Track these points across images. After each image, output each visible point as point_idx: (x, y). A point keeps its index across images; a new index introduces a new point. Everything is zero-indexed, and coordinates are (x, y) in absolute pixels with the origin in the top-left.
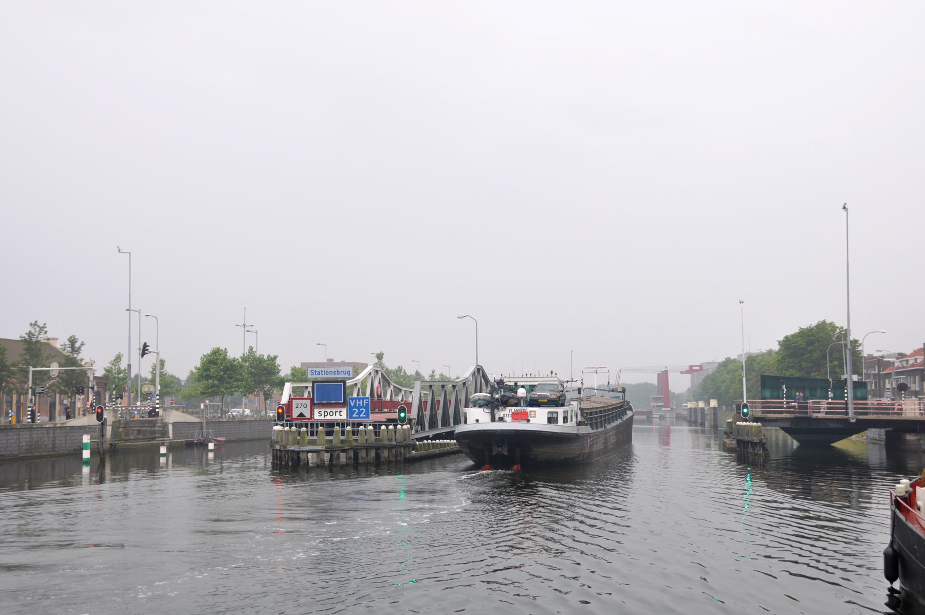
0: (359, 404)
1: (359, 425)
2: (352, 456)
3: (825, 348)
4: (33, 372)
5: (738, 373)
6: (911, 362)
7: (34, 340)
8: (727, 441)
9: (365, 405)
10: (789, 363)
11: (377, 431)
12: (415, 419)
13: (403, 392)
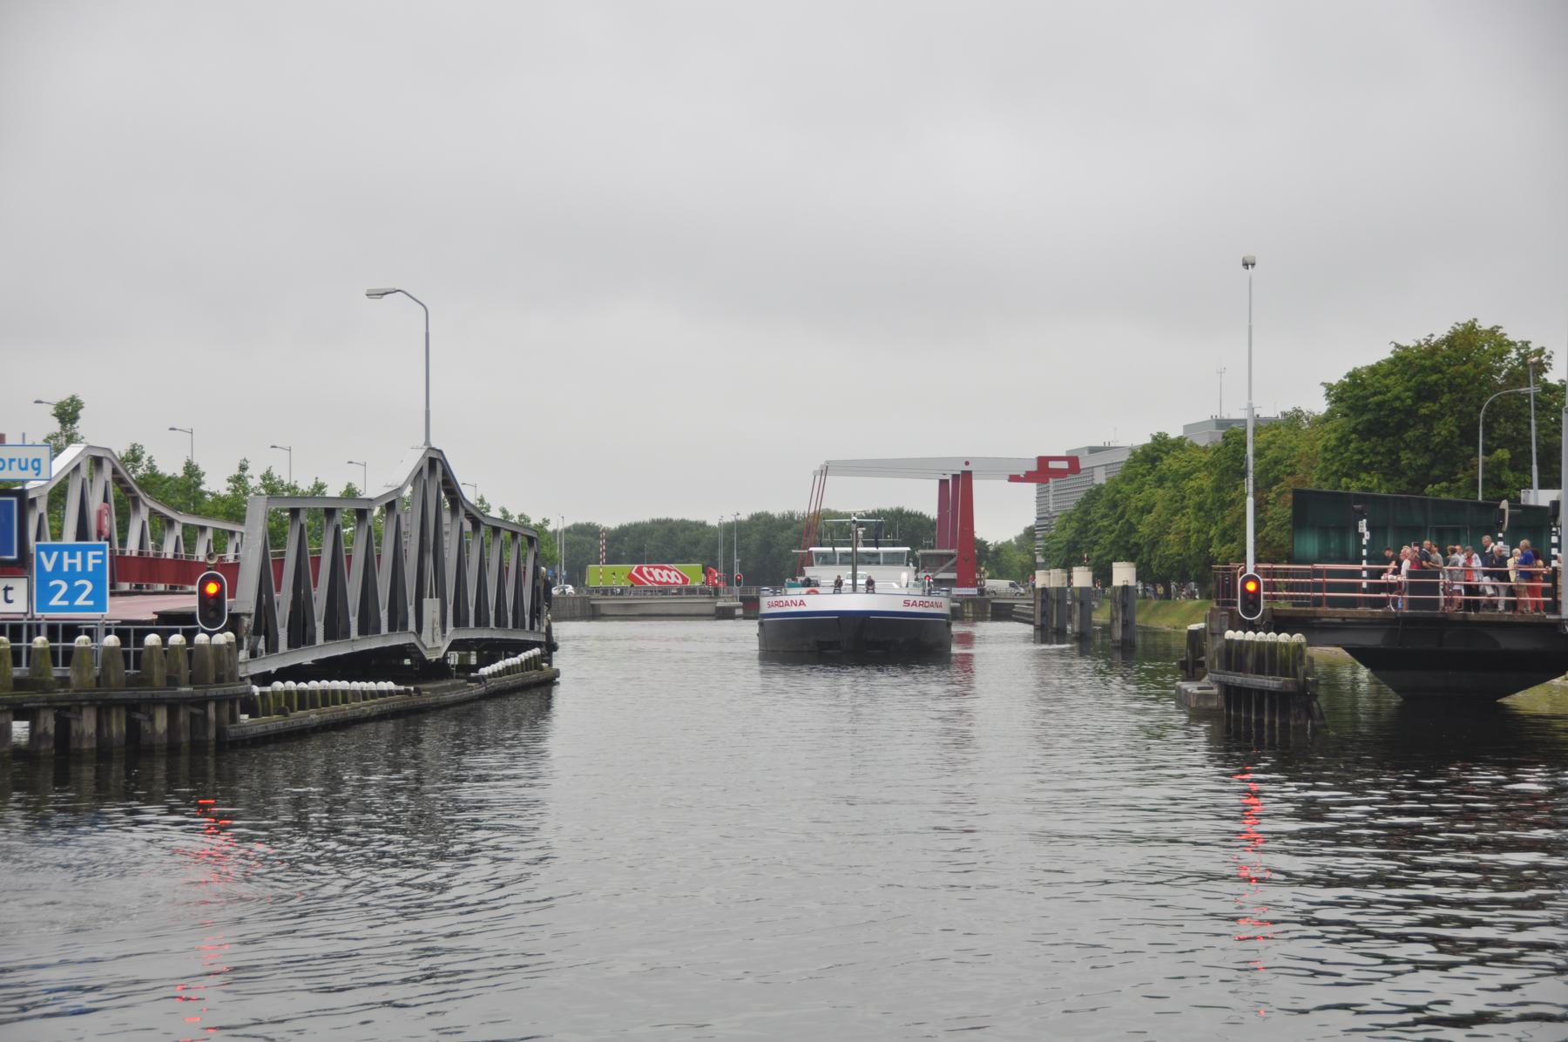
0: (72, 566)
1: (72, 631)
2: (52, 731)
3: (1472, 408)
5: (1192, 483)
9: (90, 569)
10: (1361, 452)
11: (129, 652)
12: (249, 615)
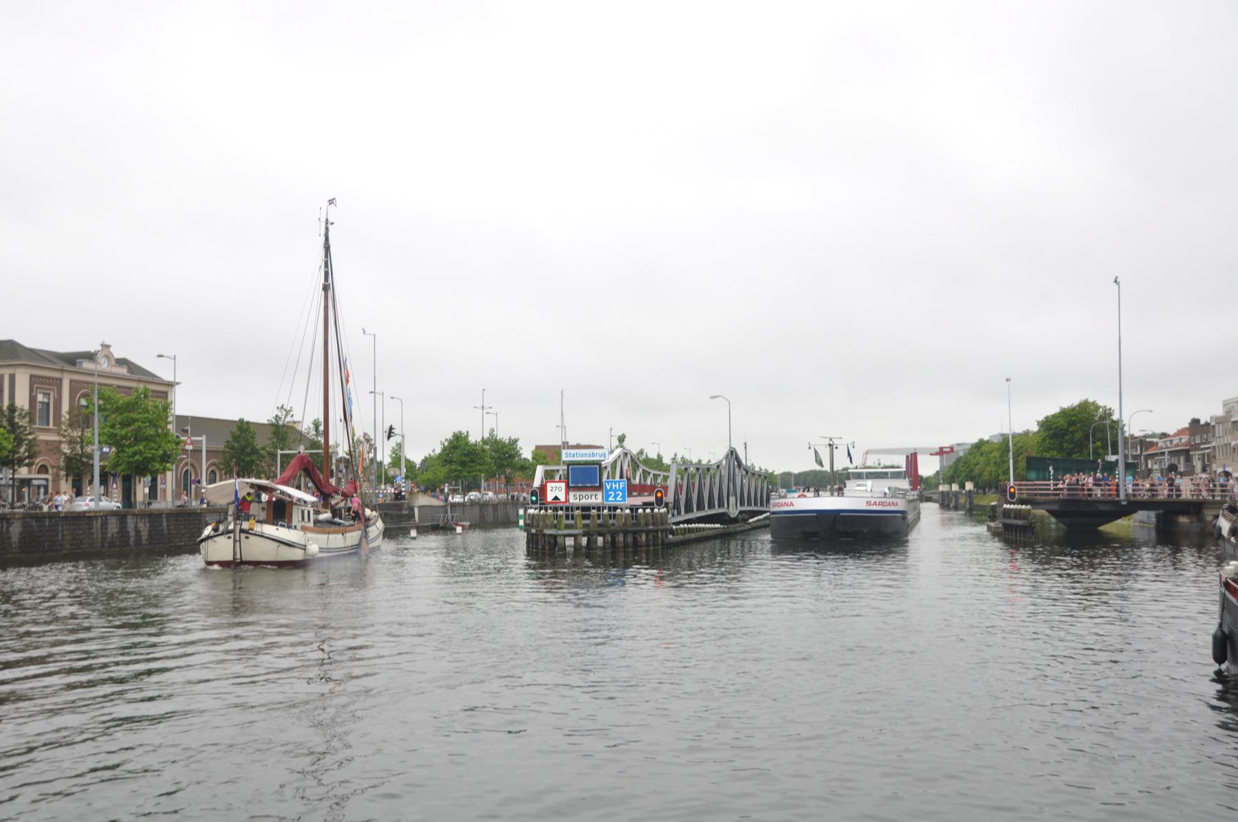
1: (615, 508)
4: (282, 455)
6: (1175, 442)
7: (281, 423)
8: (992, 524)
13: (652, 475)
